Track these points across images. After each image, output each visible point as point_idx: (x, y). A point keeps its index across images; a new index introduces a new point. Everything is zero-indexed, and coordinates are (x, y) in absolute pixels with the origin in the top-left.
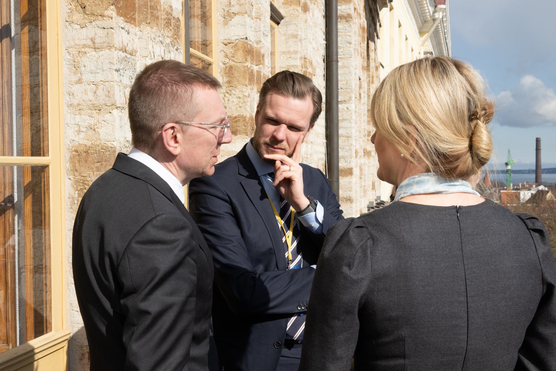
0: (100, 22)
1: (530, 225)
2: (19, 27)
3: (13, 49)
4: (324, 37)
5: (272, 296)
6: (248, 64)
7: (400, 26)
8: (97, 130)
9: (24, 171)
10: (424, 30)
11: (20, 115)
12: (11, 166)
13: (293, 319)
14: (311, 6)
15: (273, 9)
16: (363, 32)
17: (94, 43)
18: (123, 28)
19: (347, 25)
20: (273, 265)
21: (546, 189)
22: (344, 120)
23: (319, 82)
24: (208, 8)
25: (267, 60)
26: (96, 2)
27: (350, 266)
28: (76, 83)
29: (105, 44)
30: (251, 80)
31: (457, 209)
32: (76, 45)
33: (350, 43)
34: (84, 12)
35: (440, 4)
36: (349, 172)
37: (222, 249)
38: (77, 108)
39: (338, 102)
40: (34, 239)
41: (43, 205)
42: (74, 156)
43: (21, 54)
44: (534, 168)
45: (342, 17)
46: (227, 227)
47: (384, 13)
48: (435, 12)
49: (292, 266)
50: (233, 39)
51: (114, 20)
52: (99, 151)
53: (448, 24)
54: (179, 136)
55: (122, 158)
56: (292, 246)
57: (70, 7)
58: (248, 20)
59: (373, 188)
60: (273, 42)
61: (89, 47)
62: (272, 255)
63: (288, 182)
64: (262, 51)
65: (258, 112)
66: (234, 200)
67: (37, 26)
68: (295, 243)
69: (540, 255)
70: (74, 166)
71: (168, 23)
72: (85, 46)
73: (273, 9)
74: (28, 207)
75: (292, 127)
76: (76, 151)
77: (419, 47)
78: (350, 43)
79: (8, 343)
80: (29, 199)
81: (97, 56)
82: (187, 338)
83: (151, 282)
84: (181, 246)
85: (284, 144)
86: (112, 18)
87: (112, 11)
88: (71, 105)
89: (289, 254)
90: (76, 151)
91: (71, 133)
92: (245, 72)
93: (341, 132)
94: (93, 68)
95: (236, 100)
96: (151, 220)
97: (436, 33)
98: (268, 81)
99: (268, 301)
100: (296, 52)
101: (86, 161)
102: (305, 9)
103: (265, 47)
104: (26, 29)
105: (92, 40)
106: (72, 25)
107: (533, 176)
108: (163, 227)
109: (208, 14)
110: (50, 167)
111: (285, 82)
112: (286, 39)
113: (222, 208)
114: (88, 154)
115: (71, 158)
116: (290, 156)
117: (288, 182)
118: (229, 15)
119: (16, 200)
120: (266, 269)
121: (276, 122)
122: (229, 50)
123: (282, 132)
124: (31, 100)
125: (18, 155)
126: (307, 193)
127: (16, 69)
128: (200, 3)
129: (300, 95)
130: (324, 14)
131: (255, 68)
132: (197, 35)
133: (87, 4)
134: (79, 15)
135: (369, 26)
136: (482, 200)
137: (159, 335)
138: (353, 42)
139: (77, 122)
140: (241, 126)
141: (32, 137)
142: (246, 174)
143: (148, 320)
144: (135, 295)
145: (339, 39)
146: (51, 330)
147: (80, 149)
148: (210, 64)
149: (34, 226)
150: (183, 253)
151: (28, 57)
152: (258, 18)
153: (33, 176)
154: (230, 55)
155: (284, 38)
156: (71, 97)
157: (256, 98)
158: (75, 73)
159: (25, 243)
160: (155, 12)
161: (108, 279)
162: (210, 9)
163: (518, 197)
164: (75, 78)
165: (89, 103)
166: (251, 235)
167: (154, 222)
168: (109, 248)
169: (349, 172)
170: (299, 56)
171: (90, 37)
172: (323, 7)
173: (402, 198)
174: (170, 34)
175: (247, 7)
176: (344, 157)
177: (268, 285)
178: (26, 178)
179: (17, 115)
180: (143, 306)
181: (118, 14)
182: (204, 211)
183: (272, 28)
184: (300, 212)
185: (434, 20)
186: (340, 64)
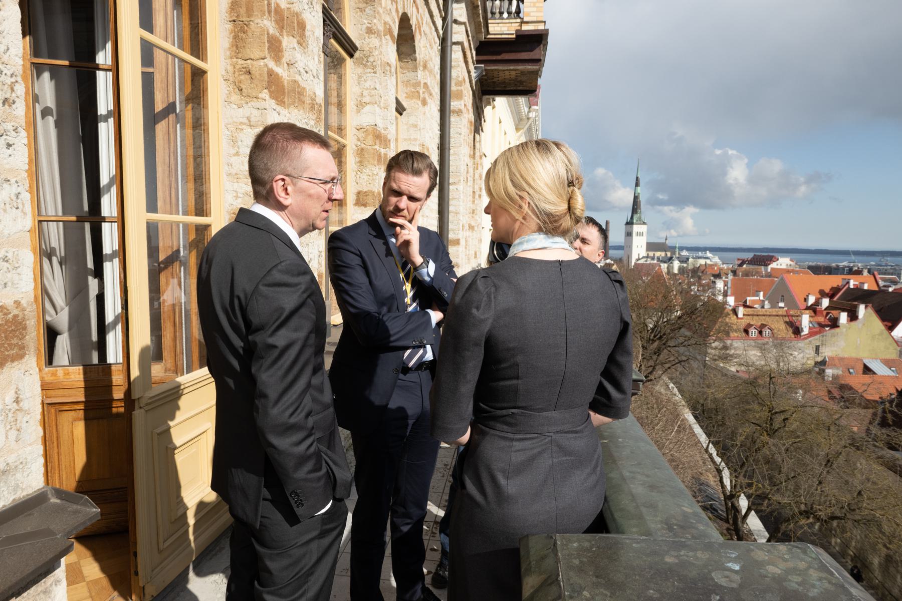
0: (255, 103)
1: (613, 277)
2: (183, 105)
5: (392, 332)
6: (377, 147)
10: (520, 127)
13: (409, 351)
14: (429, 101)
15: (398, 102)
20: (395, 307)
22: (454, 199)
23: (435, 158)
25: (393, 145)
27: (478, 308)
30: (379, 160)
31: (560, 263)
36: (457, 242)
37: (353, 294)
39: (449, 184)
46: (359, 276)
48: (529, 112)
49: (410, 309)
50: (364, 125)
53: (539, 123)
54: (290, 189)
56: (410, 294)
58: (377, 109)
59: (475, 257)
60: (397, 130)
61: (245, 124)
62: (393, 300)
63: (407, 243)
64: (389, 137)
65: (385, 184)
66: (364, 255)
67: (199, 104)
68: (412, 293)
71: (312, 107)
72: (241, 123)
73: (398, 102)
75: (412, 198)
77: (516, 138)
82: (309, 370)
83: (277, 320)
84: (303, 288)
85: (405, 213)
87: (265, 94)
89: (408, 300)
93: (451, 208)
95: (366, 178)
96: (276, 266)
98: (393, 158)
99: (390, 336)
100: (415, 140)
102: (424, 103)
103: (391, 134)
104: (190, 107)
108: (287, 272)
111: (404, 161)
113: (355, 261)
116: (410, 222)
117: (407, 243)
118: (361, 105)
119: (182, 254)
120: (389, 311)
121: (399, 194)
122: (361, 134)
123: (404, 202)
125: (184, 214)
126: (421, 253)
129: (417, 173)
131: (383, 151)
132: (334, 121)
133: (243, 87)
135: (476, 121)
137: (285, 366)
140: (370, 199)
141: (196, 200)
142: (375, 234)
143: (276, 353)
144: (262, 332)
148: (344, 146)
150: (305, 295)
152: (386, 108)
153: (197, 234)
154: (362, 139)
157: (383, 175)
158: (233, 147)
161: (236, 318)
164: (233, 151)
166: (377, 283)
167: (279, 267)
168: (239, 292)
169: (457, 242)
170: (418, 142)
172: (438, 103)
174: (314, 117)
176: (453, 230)
177: (388, 324)
180: (271, 341)
182: (339, 263)
183: (397, 118)
184: (416, 269)
185: (528, 119)
186: (451, 151)
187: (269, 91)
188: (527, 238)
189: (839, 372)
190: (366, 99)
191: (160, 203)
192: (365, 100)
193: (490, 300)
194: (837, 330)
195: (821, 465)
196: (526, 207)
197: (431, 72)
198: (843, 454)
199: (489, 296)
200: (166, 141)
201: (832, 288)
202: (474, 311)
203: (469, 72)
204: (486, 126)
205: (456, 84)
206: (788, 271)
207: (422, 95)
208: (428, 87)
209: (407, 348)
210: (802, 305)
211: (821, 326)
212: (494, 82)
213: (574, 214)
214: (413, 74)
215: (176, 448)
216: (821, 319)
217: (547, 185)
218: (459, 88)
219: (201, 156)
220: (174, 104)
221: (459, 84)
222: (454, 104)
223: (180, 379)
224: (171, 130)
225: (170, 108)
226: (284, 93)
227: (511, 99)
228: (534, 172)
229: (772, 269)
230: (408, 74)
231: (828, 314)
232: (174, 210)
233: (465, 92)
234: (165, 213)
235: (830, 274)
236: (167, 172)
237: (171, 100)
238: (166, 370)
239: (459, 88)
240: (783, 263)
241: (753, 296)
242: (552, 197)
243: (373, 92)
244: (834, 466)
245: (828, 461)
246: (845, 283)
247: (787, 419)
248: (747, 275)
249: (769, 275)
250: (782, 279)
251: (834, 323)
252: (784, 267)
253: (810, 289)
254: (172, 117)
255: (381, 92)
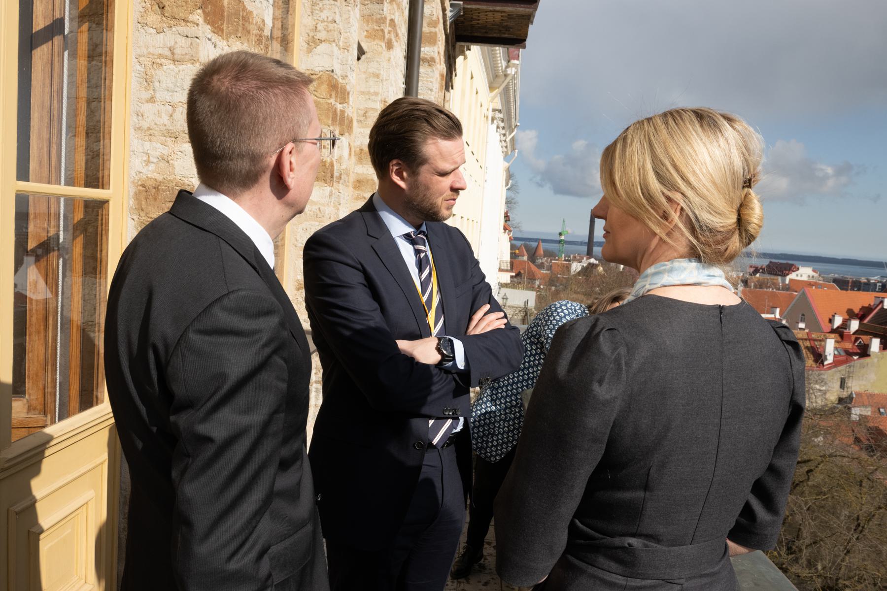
0: (182, 29)
2: (76, 24)
3: (64, 50)
4: (403, 80)
6: (332, 101)
7: (472, 78)
8: (171, 162)
9: (74, 205)
10: (496, 85)
11: (70, 134)
12: (58, 198)
16: (442, 79)
17: (173, 54)
18: (209, 40)
19: (429, 70)
21: (597, 262)
24: (290, 30)
26: (179, 3)
28: (147, 102)
29: (187, 57)
31: (721, 309)
32: (150, 53)
33: (431, 90)
34: (163, 14)
35: (514, 59)
38: (148, 133)
40: (84, 290)
41: (99, 249)
42: (140, 192)
43: (76, 58)
44: (587, 240)
45: (425, 60)
47: (460, 60)
48: (507, 67)
50: (317, 69)
51: (200, 28)
52: (173, 188)
53: (518, 82)
55: (184, 197)
57: (144, 4)
58: (336, 49)
61: (166, 58)
66: (369, 269)
67: (99, 24)
69: (795, 373)
70: (140, 204)
72: (161, 56)
74: (78, 250)
76: (143, 186)
78: (431, 90)
79: (45, 414)
80: (80, 240)
81: (176, 70)
86: (198, 25)
87: (198, 16)
88: (139, 128)
90: (143, 186)
91: (137, 163)
92: (328, 110)
94: (171, 85)
97: (506, 89)
100: (376, 94)
101: (155, 199)
104: (85, 27)
105: (171, 49)
106: (146, 28)
107: (585, 248)
109: (290, 37)
110: (111, 203)
112: (366, 78)
113: (356, 278)
114: (158, 190)
115: (136, 194)
118: (314, 42)
119: (61, 240)
124: (87, 116)
125: (67, 183)
127: (69, 76)
128: (280, 24)
130: (405, 54)
131: (339, 107)
133: (167, 4)
134: (155, 17)
136: (739, 301)
138: (434, 90)
139: (146, 151)
141: (86, 163)
145: (420, 84)
146: (103, 401)
147: (149, 184)
149: (85, 274)
151: (86, 63)
152: (346, 49)
153: (86, 212)
155: (363, 76)
156: (140, 118)
158: (146, 89)
159: (72, 294)
160: (247, 24)
162: (293, 31)
163: (568, 268)
164: (146, 95)
165: (163, 128)
171: (169, 46)
172: (404, 46)
173: (649, 291)
175: (336, 34)
178: (76, 214)
179: (67, 135)
181: (205, 20)
182: (328, 281)
185: (506, 76)
187: (204, 12)
188: (669, 265)
189: (868, 412)
190: (322, 35)
191: (33, 165)
192: (319, 36)
193: (619, 369)
194: (866, 360)
195: (849, 529)
196: (675, 216)
197: (399, 5)
198: (877, 516)
199: (617, 361)
200: (48, 75)
201: (863, 308)
202: (596, 387)
203: (444, 10)
204: (457, 81)
205: (429, 25)
206: (810, 284)
207: (387, 36)
208: (395, 26)
209: (430, 418)
210: (826, 327)
211: (849, 354)
212: (472, 26)
213: (747, 231)
214: (377, 6)
215: (42, 531)
216: (848, 345)
217: (714, 183)
218: (433, 30)
219: (98, 99)
220: (61, 21)
221: (433, 24)
222: (426, 51)
223: (48, 430)
224: (56, 59)
225: (55, 28)
226: (222, 17)
227: (486, 48)
228: (695, 162)
229: (791, 280)
230: (370, 6)
231: (857, 339)
232: (53, 179)
233: (439, 35)
234: (37, 181)
235: (859, 290)
236: (46, 120)
237: (58, 15)
238: (30, 408)
239: (433, 30)
240: (804, 273)
241: (768, 313)
242: (720, 203)
243: (331, 26)
244: (866, 532)
245: (859, 525)
246: (878, 302)
247: (811, 471)
248: (761, 287)
249: (787, 288)
250: (804, 293)
251: (864, 351)
252: (805, 278)
253: (835, 308)
254: (58, 40)
255: (341, 26)
